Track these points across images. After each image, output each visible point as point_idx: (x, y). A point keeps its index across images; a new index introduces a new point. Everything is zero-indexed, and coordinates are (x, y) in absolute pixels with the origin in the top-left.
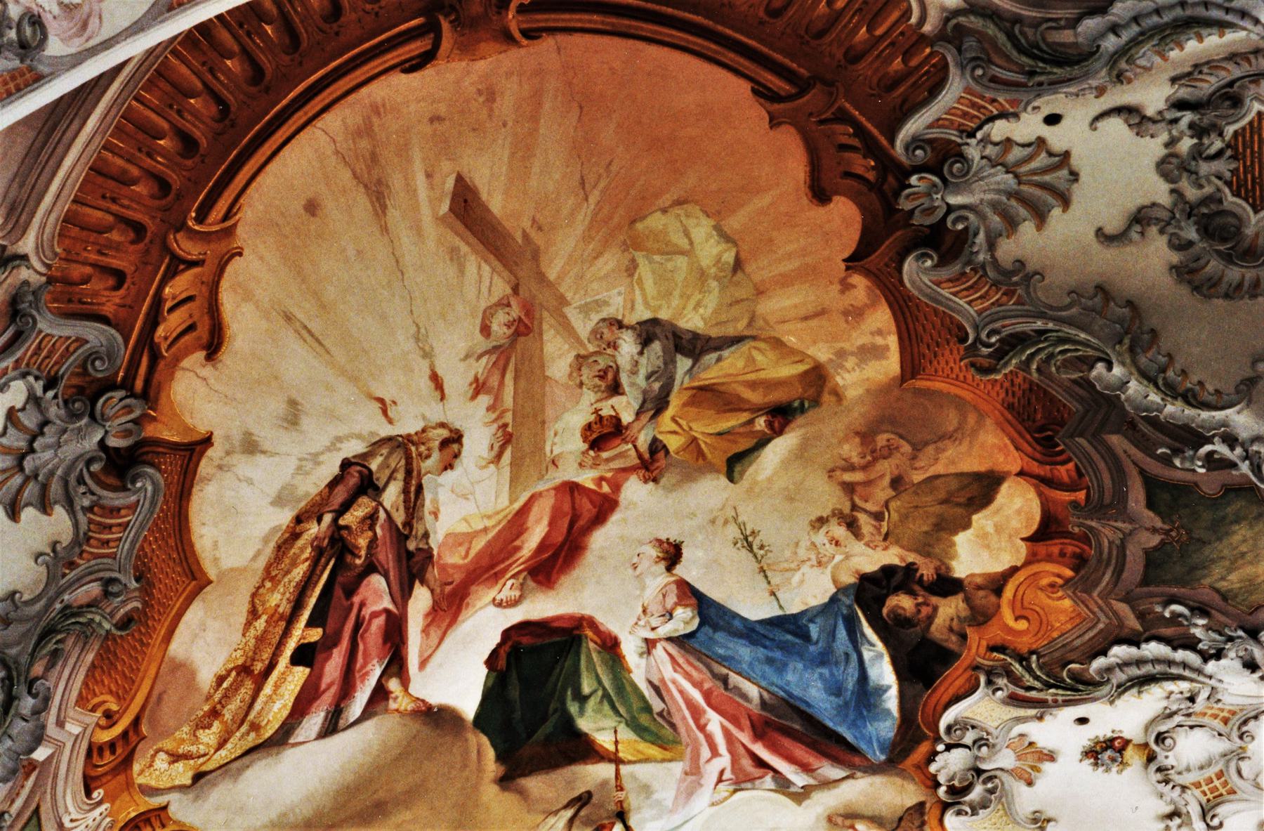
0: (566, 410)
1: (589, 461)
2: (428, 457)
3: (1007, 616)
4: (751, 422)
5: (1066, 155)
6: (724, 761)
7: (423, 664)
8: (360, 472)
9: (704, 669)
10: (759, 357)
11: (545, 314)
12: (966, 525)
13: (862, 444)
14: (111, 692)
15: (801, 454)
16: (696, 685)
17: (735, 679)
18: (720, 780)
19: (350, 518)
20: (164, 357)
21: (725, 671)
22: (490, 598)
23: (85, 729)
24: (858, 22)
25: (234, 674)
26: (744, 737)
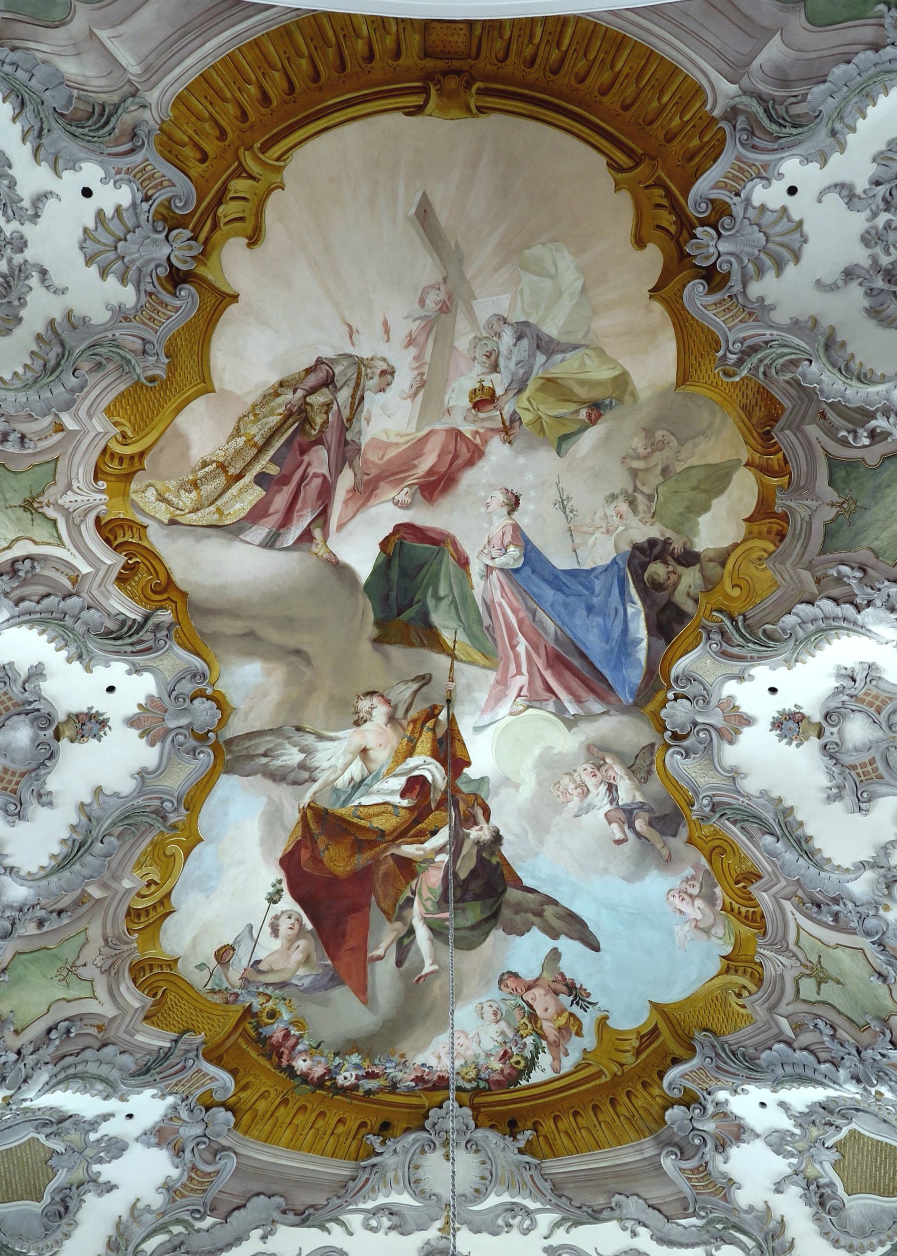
0: (462, 375)
1: (471, 418)
2: (371, 378)
3: (727, 583)
4: (577, 412)
5: (800, 223)
6: (523, 680)
7: (340, 527)
8: (327, 371)
9: (521, 600)
10: (588, 362)
11: (460, 302)
12: (706, 508)
13: (646, 437)
14: (130, 421)
15: (606, 441)
16: (515, 611)
17: (540, 613)
18: (519, 695)
19: (313, 399)
20: (221, 229)
21: (535, 606)
22: (391, 496)
23: (106, 433)
24: (675, 112)
25: (214, 465)
26: (540, 663)
